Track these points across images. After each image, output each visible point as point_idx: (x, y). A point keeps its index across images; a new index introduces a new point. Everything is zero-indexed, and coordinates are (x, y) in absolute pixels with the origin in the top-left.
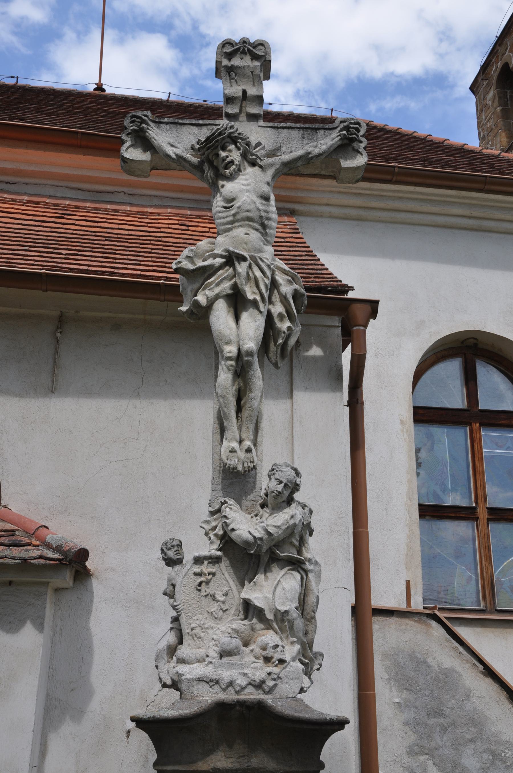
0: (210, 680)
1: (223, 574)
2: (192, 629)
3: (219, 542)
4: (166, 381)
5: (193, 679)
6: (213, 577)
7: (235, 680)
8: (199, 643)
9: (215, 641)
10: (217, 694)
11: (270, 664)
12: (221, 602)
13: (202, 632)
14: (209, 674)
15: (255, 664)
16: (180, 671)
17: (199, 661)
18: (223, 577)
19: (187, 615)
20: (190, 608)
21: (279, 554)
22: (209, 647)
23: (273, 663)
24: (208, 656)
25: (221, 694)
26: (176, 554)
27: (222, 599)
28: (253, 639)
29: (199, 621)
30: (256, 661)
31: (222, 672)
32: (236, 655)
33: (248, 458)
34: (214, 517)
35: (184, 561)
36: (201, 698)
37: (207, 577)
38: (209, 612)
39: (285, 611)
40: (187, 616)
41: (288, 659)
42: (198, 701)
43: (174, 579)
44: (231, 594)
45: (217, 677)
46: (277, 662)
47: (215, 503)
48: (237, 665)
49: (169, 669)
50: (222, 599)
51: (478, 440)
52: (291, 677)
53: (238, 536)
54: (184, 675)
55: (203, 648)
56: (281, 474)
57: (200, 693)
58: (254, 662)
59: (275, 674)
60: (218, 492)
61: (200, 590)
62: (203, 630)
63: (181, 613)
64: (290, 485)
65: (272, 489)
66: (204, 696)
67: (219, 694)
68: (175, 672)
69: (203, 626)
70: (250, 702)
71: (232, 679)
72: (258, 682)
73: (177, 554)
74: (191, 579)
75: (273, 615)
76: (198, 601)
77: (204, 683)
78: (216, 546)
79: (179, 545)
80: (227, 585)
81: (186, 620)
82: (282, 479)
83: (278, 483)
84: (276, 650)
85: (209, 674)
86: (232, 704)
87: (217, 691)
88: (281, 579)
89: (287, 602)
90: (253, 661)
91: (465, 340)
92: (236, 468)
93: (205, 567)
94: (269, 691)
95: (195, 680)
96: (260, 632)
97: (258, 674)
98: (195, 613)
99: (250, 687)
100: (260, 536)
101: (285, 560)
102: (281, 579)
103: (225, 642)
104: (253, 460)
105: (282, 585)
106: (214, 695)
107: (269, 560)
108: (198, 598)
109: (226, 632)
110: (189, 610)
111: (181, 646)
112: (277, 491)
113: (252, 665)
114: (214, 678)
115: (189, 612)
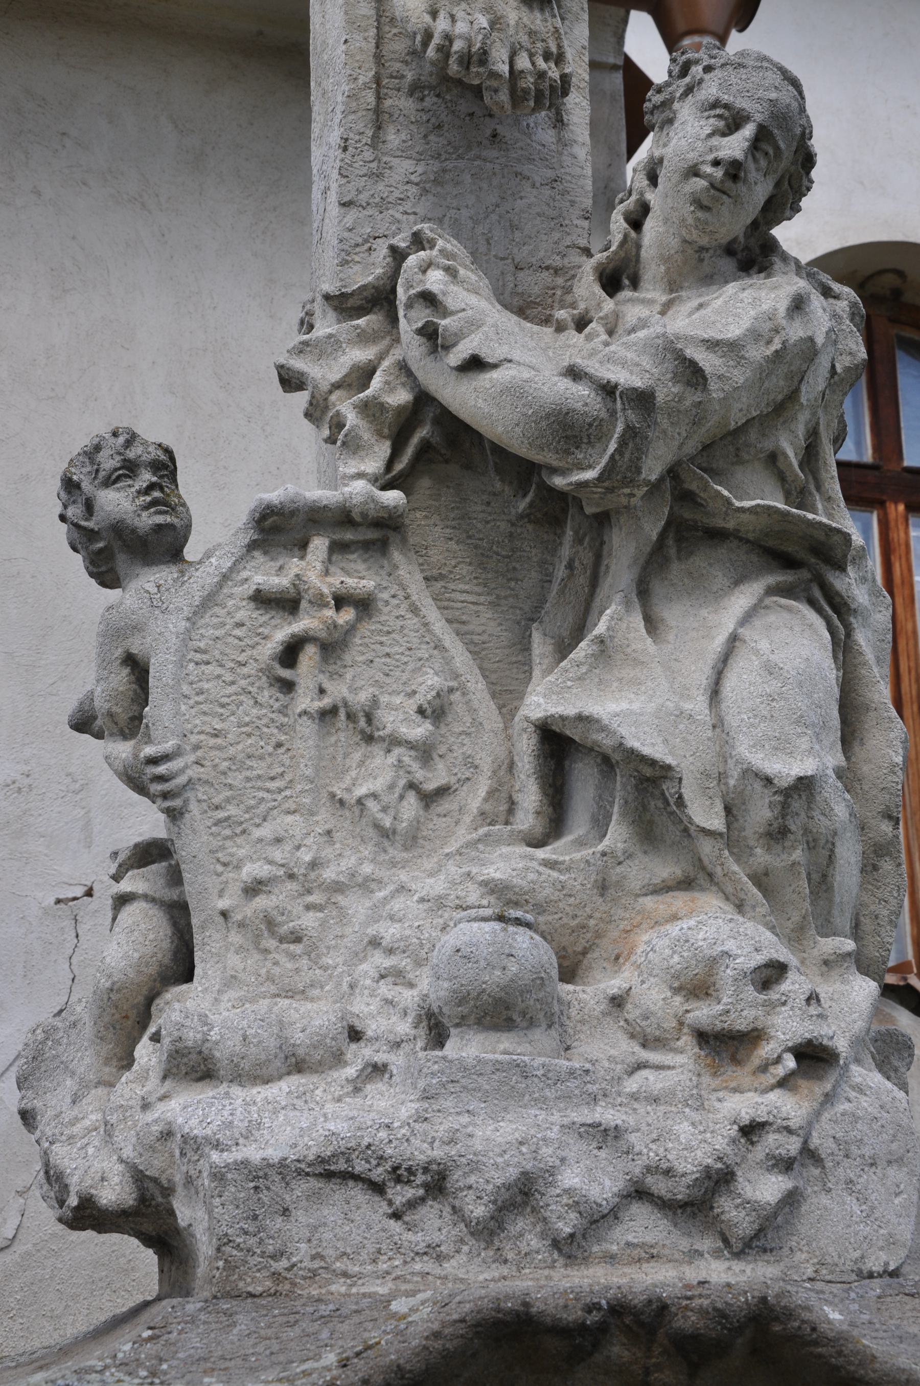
0: (395, 1169)
1: (415, 610)
2: (254, 889)
3: (384, 449)
4: (38, 194)
5: (282, 1164)
6: (359, 619)
7: (552, 1171)
8: (289, 966)
9: (390, 951)
10: (440, 1258)
11: (742, 1075)
12: (411, 745)
13: (308, 907)
14: (383, 1134)
15: (645, 1073)
16: (194, 1122)
17: (298, 1066)
18: (412, 622)
19: (221, 814)
20: (236, 779)
21: (728, 502)
22: (352, 987)
23: (764, 1068)
24: (355, 1035)
25: (462, 1258)
26: (146, 507)
27: (419, 730)
28: (604, 942)
29: (288, 847)
30: (653, 1057)
31: (465, 1119)
32: (532, 1023)
33: (531, 33)
34: (361, 322)
35: (191, 552)
36: (339, 1287)
37: (330, 613)
38: (341, 802)
39: (800, 779)
40: (218, 823)
41: (842, 1045)
42: (325, 1309)
43: (137, 628)
44: (460, 708)
45: (438, 1153)
46: (790, 1063)
47: (357, 268)
48: (551, 1078)
49: (113, 1119)
50: (419, 730)
51: (903, 547)
52: (867, 1151)
53: (515, 391)
54: (217, 1146)
55: (316, 992)
56: (733, 80)
57: (330, 1252)
58: (641, 1066)
59: (789, 1130)
60: (369, 211)
61: (288, 686)
62: (310, 899)
63: (186, 802)
64: (782, 145)
65: (691, 155)
66: (360, 1276)
67: (447, 1257)
68: (156, 1128)
69: (313, 875)
70: (702, 1311)
71: (529, 1166)
72: (689, 1179)
73: (155, 503)
74: (240, 625)
75: (719, 807)
76: (279, 745)
77: (358, 1194)
78: (373, 464)
79: (165, 467)
80: (437, 666)
81: (215, 843)
82: (741, 103)
83: (721, 124)
84: (774, 995)
85: (383, 1134)
86: (582, 1328)
87: (436, 1238)
88: (741, 630)
89: (799, 736)
90: (631, 1059)
91: (871, 277)
92: (483, 57)
93: (319, 566)
94: (760, 1232)
95: (300, 1172)
96: (648, 902)
97: (684, 1129)
98: (263, 808)
99: (641, 1213)
100: (638, 382)
101: (748, 541)
102: (741, 630)
103: (472, 944)
104: (559, 47)
105: (757, 652)
106: (418, 1267)
107: (662, 536)
108: (281, 727)
109: (452, 901)
110: (230, 786)
111: (185, 987)
112: (716, 163)
113: (632, 1085)
114: (422, 1158)
115: (228, 800)
